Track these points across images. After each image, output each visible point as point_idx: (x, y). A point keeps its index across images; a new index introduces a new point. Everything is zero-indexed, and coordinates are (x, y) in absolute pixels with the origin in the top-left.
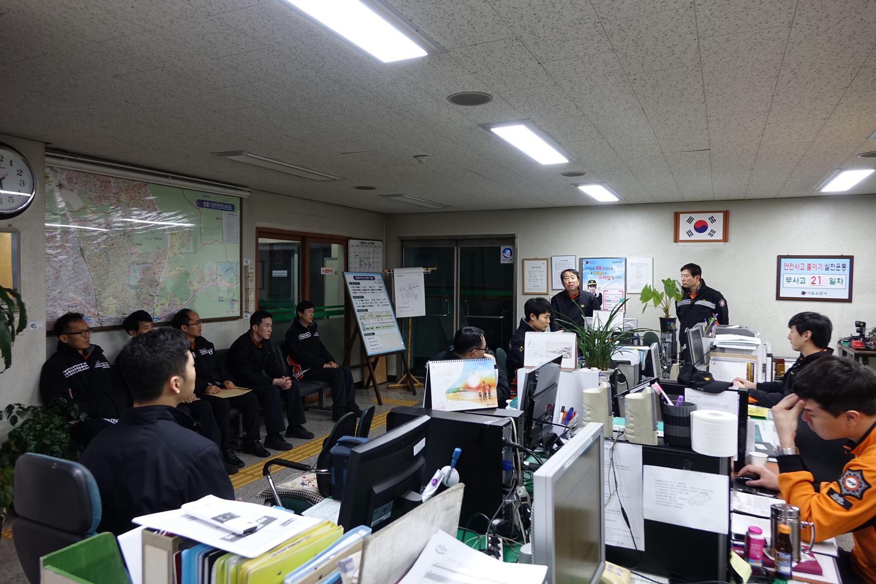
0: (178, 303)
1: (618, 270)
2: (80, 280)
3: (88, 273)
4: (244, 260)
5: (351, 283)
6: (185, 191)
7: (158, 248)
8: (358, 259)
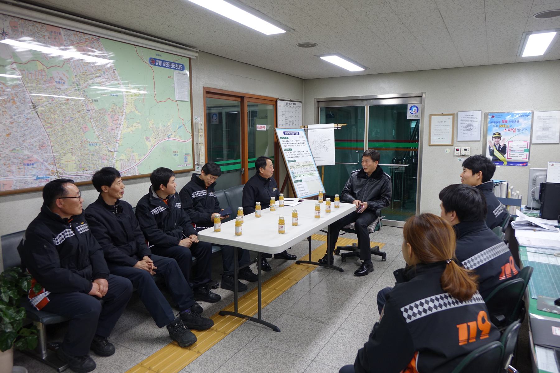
0: (137, 158)
1: (524, 123)
2: (34, 137)
3: (43, 129)
4: (194, 118)
5: (282, 138)
7: (115, 104)
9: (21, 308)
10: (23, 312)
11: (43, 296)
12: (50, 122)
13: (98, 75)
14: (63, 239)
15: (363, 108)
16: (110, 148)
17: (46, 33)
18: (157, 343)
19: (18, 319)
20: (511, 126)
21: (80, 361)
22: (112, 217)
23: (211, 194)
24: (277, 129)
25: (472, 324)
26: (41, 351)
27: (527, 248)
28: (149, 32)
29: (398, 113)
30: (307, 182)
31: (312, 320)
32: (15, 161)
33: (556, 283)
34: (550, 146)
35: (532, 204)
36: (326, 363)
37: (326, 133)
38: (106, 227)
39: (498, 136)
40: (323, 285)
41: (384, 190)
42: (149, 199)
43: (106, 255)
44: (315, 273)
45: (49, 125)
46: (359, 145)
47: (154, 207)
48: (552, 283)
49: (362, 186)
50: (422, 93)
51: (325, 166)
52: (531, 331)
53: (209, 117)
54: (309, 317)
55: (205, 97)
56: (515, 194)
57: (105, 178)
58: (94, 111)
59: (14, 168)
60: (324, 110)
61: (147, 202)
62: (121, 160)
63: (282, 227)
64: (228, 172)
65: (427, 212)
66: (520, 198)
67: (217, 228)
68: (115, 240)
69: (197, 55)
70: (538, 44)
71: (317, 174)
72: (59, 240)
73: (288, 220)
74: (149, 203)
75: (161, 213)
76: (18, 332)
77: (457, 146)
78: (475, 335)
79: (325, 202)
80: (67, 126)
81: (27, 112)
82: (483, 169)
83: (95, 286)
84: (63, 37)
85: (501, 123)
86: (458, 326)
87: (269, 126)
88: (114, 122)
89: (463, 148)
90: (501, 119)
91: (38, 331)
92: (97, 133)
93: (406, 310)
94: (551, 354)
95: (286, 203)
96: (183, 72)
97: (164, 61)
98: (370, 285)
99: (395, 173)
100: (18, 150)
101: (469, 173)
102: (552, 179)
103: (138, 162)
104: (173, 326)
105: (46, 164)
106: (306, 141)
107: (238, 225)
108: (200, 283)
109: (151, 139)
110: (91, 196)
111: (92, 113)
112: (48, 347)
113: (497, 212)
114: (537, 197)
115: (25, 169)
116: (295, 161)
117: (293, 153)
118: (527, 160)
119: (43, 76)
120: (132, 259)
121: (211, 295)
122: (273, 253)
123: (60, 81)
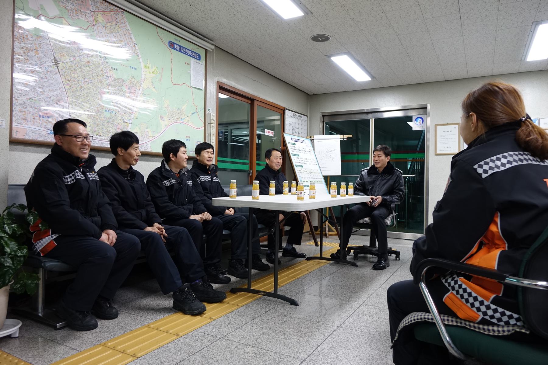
0: (151, 134)
3: (61, 85)
6: (159, 29)
11: (46, 241)
14: (73, 180)
15: (368, 121)
21: (81, 316)
22: (124, 180)
23: (215, 179)
28: (170, 16)
32: (31, 110)
36: (354, 329)
37: (334, 142)
38: (117, 190)
41: (397, 185)
45: (68, 82)
47: (167, 179)
49: (373, 182)
59: (29, 116)
61: (157, 176)
68: (124, 203)
69: (213, 47)
72: (69, 179)
75: (172, 185)
81: (48, 64)
83: (104, 237)
93: (481, 166)
98: (388, 275)
100: (35, 100)
103: (151, 138)
108: (209, 262)
109: (165, 118)
116: (302, 167)
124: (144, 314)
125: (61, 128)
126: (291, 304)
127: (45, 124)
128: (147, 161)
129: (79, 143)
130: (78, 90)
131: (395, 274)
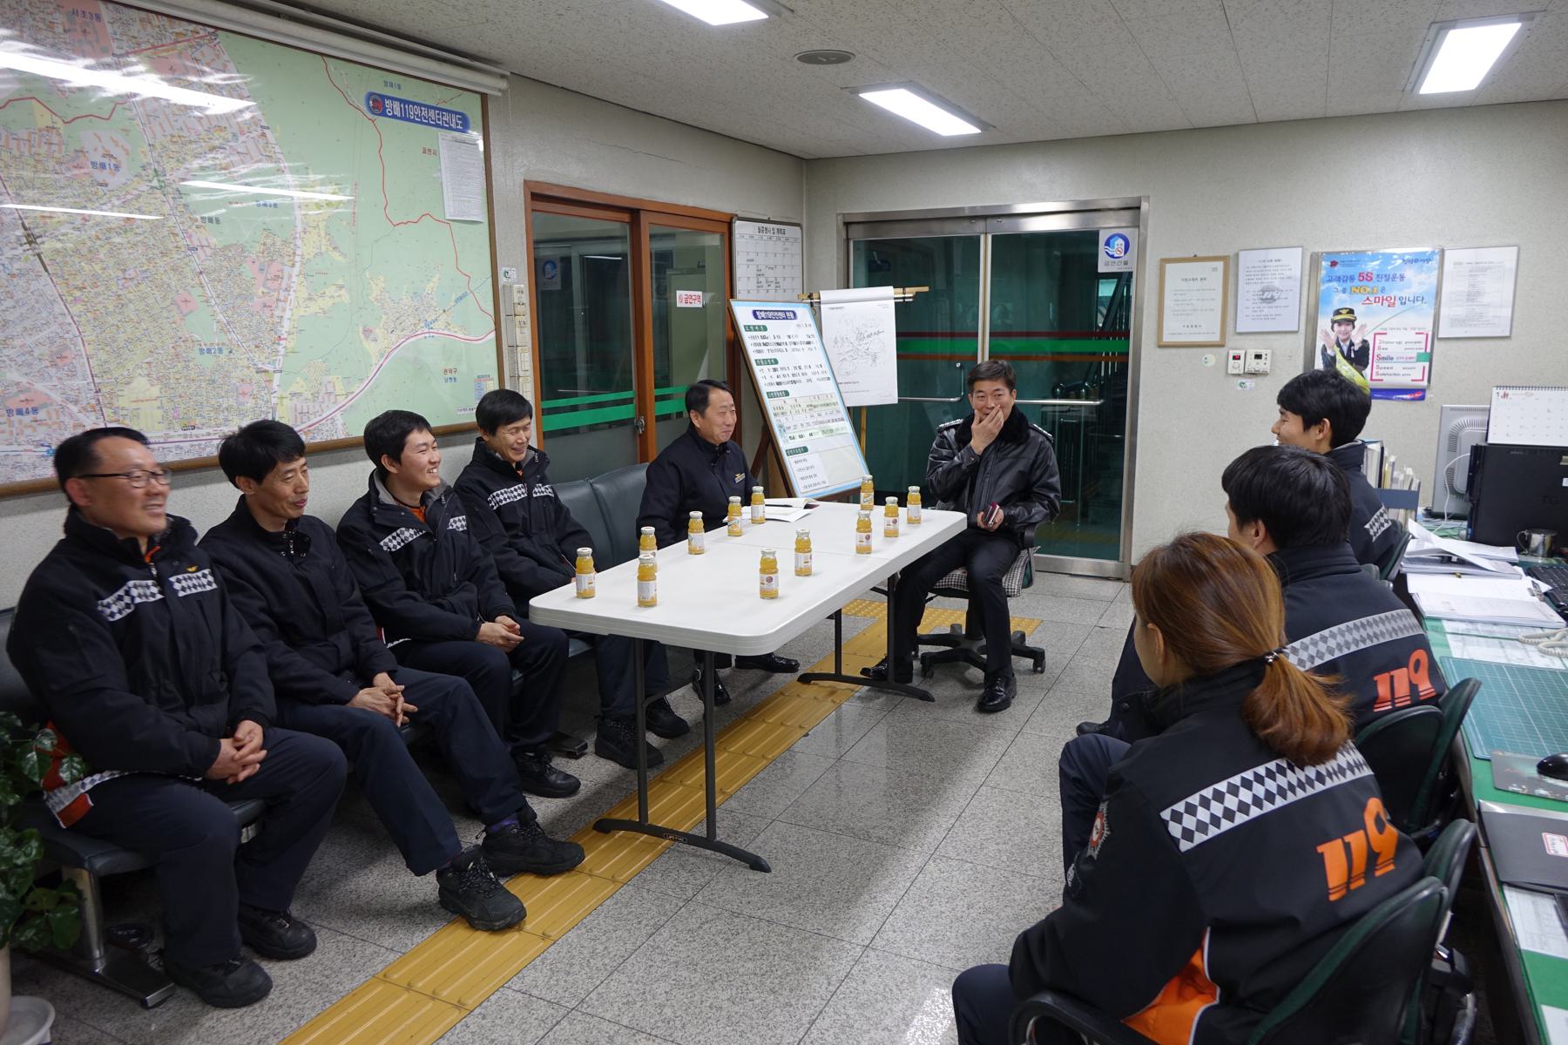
0: (340, 388)
1: (1418, 281)
3: (59, 307)
5: (748, 328)
6: (331, 63)
8: (753, 269)
9: (27, 831)
10: (34, 844)
12: (79, 283)
13: (217, 143)
15: (974, 242)
16: (260, 359)
17: (57, 15)
18: (419, 919)
19: (19, 862)
20: (1383, 290)
22: (277, 563)
23: (541, 491)
24: (734, 303)
25: (1356, 839)
26: (90, 952)
27: (1445, 623)
28: (364, 17)
29: (1071, 256)
30: (823, 452)
31: (855, 836)
33: (1535, 717)
34: (1492, 343)
35: (1448, 505)
37: (876, 309)
39: (1346, 318)
40: (879, 737)
41: (1038, 473)
42: (368, 510)
43: (273, 668)
44: (852, 703)
45: (78, 293)
46: (961, 346)
47: (389, 530)
48: (1524, 717)
50: (1139, 199)
51: (870, 408)
52: (1488, 846)
53: (539, 267)
54: (847, 828)
55: (531, 212)
56: (1401, 477)
57: (258, 452)
58: (209, 251)
60: (862, 247)
61: (369, 515)
62: (294, 394)
63: (770, 580)
64: (593, 428)
65: (1189, 531)
66: (1414, 488)
67: (586, 586)
68: (288, 631)
69: (503, 84)
70: (1466, 59)
71: (847, 426)
73: (786, 561)
74: (370, 518)
75: (408, 547)
76: (22, 901)
77: (1235, 345)
78: (1363, 868)
79: (881, 509)
80: (131, 296)
81: (9, 254)
82: (1332, 413)
84: (109, 29)
85: (1356, 283)
86: (1320, 849)
87: (709, 295)
88: (269, 283)
89: (1252, 353)
90: (1349, 271)
91: (80, 894)
92: (221, 317)
94: (1547, 906)
95: (771, 512)
96: (464, 136)
97: (409, 103)
98: (1009, 735)
99: (1062, 426)
101: (1294, 424)
102: (1499, 436)
103: (342, 400)
104: (459, 869)
105: (74, 409)
106: (816, 339)
107: (645, 575)
109: (378, 332)
110: (211, 504)
111: (203, 257)
112: (108, 939)
113: (1375, 527)
114: (1461, 483)
115: (11, 424)
116: (787, 394)
117: (780, 373)
118: (1425, 383)
119: (54, 148)
120: (345, 682)
121: (553, 777)
122: (735, 651)
123: (106, 161)
124: (368, 929)
125: (75, 457)
126: (752, 868)
127: (28, 431)
128: (339, 463)
129: (140, 492)
130: (111, 308)
131: (1020, 739)
